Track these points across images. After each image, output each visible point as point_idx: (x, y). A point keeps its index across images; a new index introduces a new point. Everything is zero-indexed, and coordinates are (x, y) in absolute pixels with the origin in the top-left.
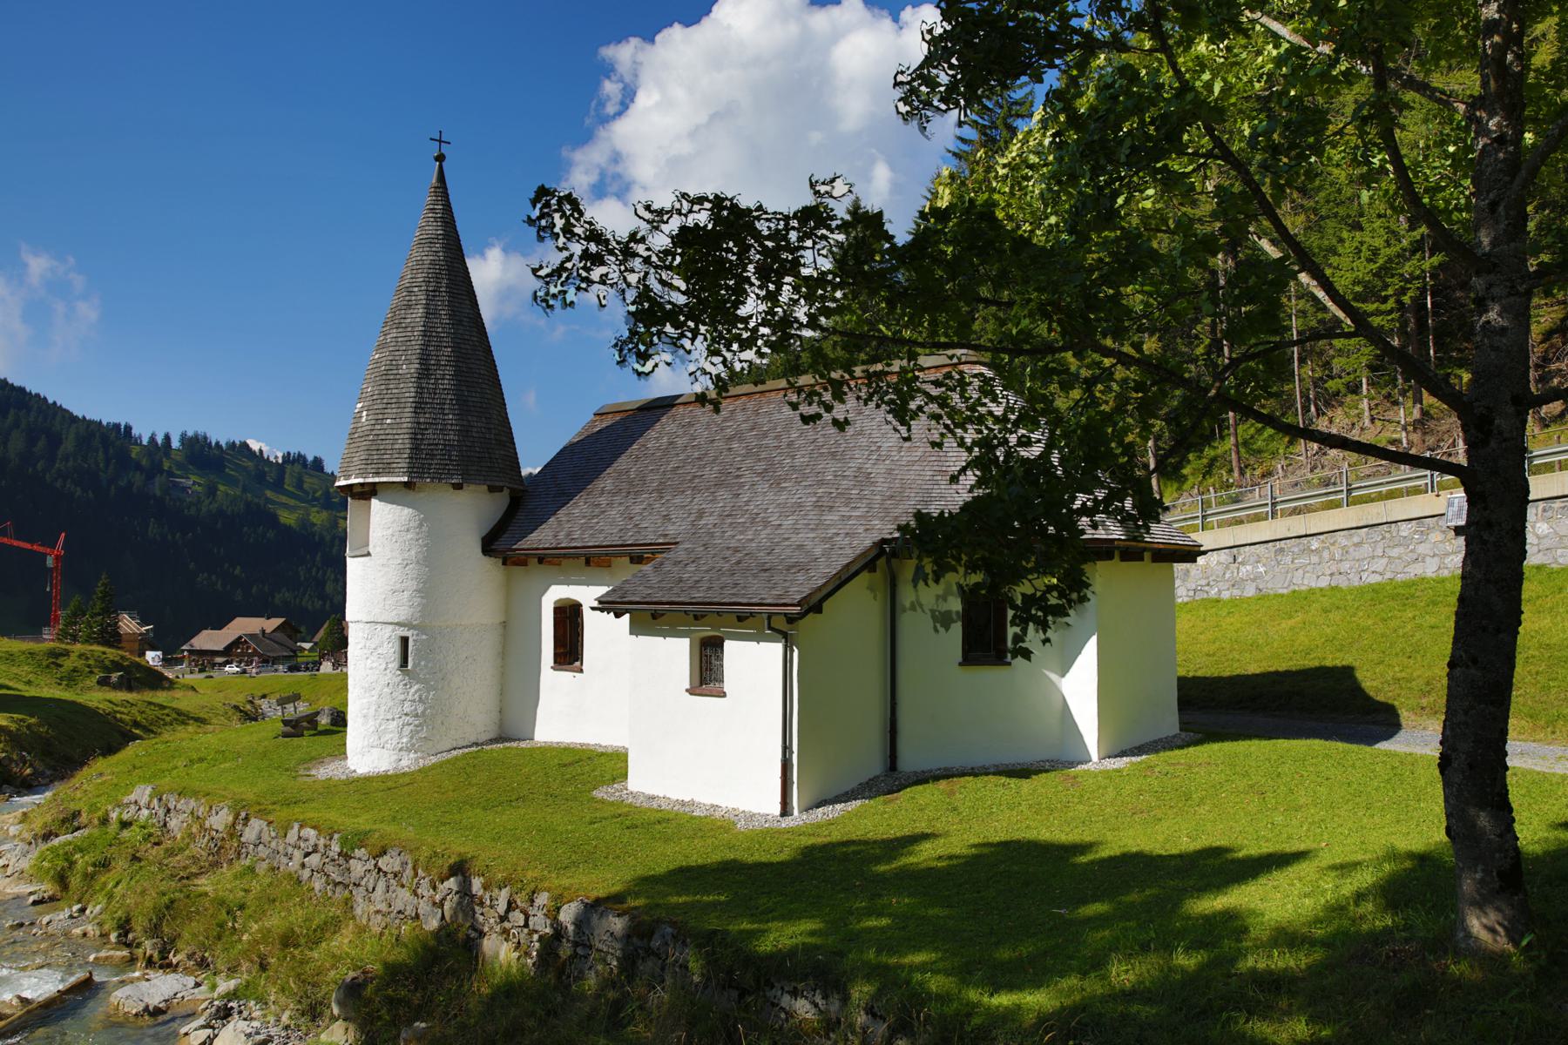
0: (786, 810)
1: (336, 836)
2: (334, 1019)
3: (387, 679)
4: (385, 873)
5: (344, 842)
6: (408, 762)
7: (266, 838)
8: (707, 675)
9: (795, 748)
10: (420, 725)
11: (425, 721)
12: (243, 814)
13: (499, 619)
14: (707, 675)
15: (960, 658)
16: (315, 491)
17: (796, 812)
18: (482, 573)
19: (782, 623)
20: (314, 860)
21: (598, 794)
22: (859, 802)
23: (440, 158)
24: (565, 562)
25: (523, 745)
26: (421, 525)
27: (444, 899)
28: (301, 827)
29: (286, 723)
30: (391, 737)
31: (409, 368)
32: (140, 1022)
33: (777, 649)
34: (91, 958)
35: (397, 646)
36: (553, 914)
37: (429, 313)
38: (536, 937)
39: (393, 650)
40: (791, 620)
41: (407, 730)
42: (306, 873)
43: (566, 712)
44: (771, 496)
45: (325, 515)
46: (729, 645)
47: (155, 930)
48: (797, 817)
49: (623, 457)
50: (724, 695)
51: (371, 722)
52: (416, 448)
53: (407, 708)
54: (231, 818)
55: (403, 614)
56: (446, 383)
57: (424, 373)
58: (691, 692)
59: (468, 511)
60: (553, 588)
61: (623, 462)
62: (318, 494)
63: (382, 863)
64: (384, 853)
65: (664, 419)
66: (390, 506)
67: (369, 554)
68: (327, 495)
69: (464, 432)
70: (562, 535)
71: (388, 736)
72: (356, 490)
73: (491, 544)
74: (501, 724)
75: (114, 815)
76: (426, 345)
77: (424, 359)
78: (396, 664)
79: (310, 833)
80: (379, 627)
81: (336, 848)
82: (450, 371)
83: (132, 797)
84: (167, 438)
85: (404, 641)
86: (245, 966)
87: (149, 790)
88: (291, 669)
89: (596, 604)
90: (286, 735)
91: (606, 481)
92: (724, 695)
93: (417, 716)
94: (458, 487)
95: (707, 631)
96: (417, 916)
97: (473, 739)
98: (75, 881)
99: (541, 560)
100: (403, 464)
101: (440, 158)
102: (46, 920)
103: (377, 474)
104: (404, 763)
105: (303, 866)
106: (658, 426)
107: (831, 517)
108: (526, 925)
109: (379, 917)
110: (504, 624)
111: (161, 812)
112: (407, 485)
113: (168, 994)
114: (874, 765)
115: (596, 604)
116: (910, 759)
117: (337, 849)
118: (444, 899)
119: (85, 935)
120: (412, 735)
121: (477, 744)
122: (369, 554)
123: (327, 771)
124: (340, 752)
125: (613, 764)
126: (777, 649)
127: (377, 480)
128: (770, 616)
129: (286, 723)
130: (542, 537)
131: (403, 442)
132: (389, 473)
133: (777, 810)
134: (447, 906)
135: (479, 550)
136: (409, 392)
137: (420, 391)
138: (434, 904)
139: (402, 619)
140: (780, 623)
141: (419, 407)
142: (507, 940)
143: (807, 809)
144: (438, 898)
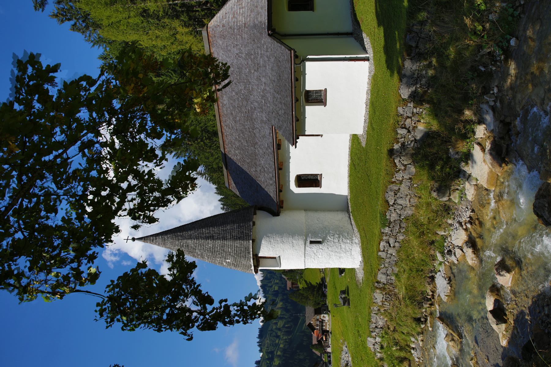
0: (367, 59)
1: (382, 231)
2: (450, 200)
3: (326, 249)
4: (395, 200)
5: (384, 225)
6: (357, 240)
7: (384, 270)
8: (318, 98)
9: (344, 56)
10: (343, 236)
11: (341, 234)
12: (376, 284)
13: (303, 212)
14: (318, 98)
15: (322, 107)
16: (267, 363)
17: (367, 55)
18: (287, 218)
19: (299, 61)
20: (392, 241)
21: (364, 144)
22: (364, 35)
23: (134, 239)
24: (281, 183)
25: (349, 197)
26: (268, 237)
27: (403, 164)
28: (380, 251)
29: (344, 305)
30: (348, 246)
31: (210, 243)
32: (454, 285)
33: (308, 64)
34: (430, 329)
35: (314, 245)
36: (404, 102)
37: (190, 238)
38: (415, 110)
39: (315, 246)
40: (296, 57)
41: (344, 240)
42: (397, 244)
43: (337, 182)
44: (255, 93)
45: (276, 360)
46: (308, 87)
47: (420, 305)
48: (370, 54)
49: (243, 168)
50: (326, 89)
51: (342, 255)
52: (240, 238)
53: (336, 241)
54: (378, 291)
55: (301, 242)
56: (216, 230)
57: (212, 238)
58: (325, 105)
59: (263, 221)
60: (291, 188)
61: (245, 167)
62: (268, 362)
63: (391, 203)
64: (387, 202)
65: (230, 156)
66: (261, 249)
67: (279, 257)
68: (268, 359)
69: (233, 222)
70: (271, 182)
71: (347, 248)
72: (256, 264)
73: (276, 214)
74: (342, 210)
75: (379, 355)
76: (202, 238)
77: (207, 238)
78: (320, 245)
79: (383, 244)
80: (306, 252)
81: (387, 230)
82: (211, 229)
83: (372, 347)
84: (218, 60)
85: (311, 242)
86: (432, 252)
87: (369, 339)
88: (330, 363)
89: (294, 146)
90: (349, 304)
91: (252, 171)
92: (326, 89)
93: (339, 237)
94: (254, 224)
95: (303, 98)
96: (410, 179)
97: (348, 218)
98: (403, 354)
99: (280, 191)
100: (245, 243)
101: (134, 239)
102: (417, 360)
103: (249, 253)
104: (357, 241)
105: (394, 247)
106: (232, 158)
107: (262, 62)
108: (411, 118)
109: (411, 200)
110: (306, 210)
111: (377, 330)
112: (253, 241)
113: (443, 279)
114: (351, 40)
115: (294, 146)
116: (348, 27)
117: (387, 228)
118: (403, 164)
119: (422, 341)
120: (346, 238)
121: (350, 215)
122: (279, 257)
123: (360, 275)
124: (353, 270)
125: (355, 138)
126: (308, 64)
127: (251, 253)
128: (295, 63)
129: (344, 305)
130: (271, 191)
131: (237, 243)
132: (248, 250)
133: (367, 62)
134: (405, 163)
135: (277, 217)
136: (219, 243)
137: (218, 239)
138: (405, 169)
139: (303, 243)
140: (298, 61)
141: (224, 238)
142: (417, 127)
143: (366, 52)
144: (403, 168)
